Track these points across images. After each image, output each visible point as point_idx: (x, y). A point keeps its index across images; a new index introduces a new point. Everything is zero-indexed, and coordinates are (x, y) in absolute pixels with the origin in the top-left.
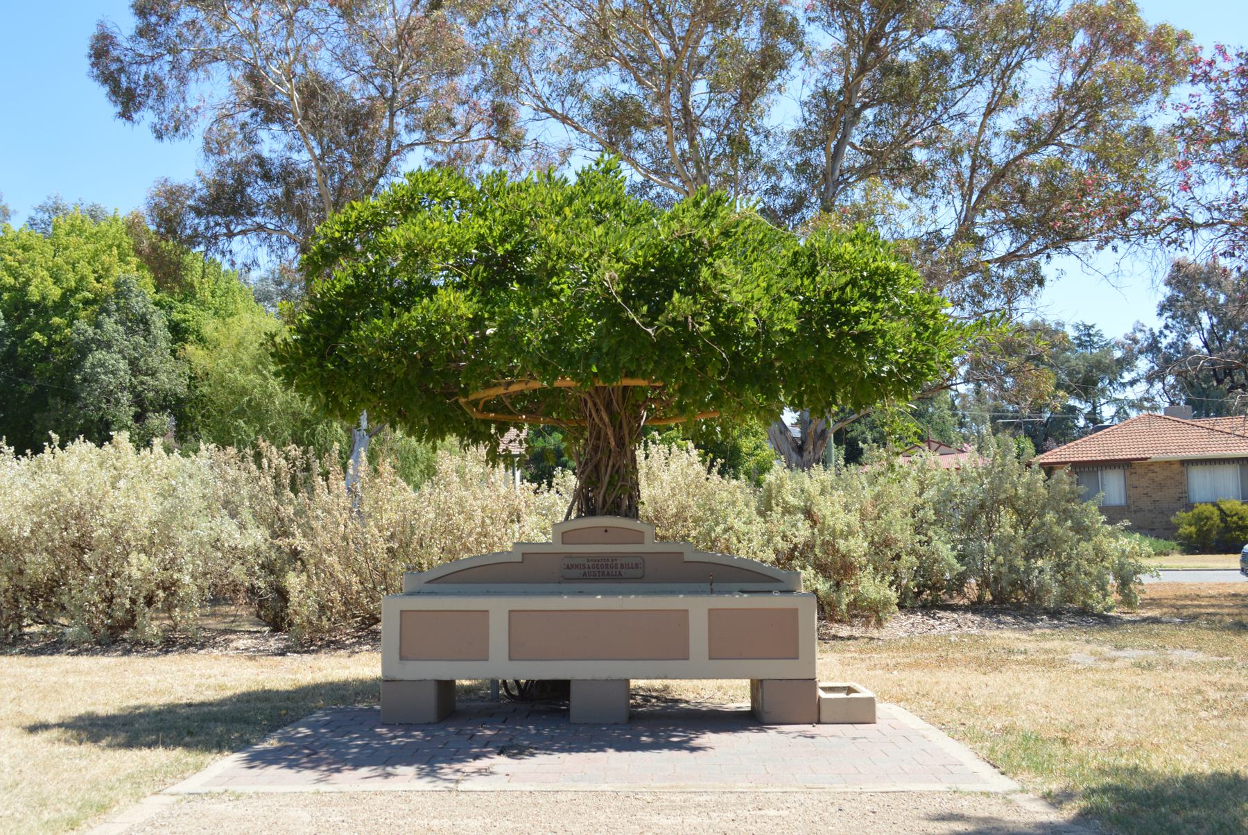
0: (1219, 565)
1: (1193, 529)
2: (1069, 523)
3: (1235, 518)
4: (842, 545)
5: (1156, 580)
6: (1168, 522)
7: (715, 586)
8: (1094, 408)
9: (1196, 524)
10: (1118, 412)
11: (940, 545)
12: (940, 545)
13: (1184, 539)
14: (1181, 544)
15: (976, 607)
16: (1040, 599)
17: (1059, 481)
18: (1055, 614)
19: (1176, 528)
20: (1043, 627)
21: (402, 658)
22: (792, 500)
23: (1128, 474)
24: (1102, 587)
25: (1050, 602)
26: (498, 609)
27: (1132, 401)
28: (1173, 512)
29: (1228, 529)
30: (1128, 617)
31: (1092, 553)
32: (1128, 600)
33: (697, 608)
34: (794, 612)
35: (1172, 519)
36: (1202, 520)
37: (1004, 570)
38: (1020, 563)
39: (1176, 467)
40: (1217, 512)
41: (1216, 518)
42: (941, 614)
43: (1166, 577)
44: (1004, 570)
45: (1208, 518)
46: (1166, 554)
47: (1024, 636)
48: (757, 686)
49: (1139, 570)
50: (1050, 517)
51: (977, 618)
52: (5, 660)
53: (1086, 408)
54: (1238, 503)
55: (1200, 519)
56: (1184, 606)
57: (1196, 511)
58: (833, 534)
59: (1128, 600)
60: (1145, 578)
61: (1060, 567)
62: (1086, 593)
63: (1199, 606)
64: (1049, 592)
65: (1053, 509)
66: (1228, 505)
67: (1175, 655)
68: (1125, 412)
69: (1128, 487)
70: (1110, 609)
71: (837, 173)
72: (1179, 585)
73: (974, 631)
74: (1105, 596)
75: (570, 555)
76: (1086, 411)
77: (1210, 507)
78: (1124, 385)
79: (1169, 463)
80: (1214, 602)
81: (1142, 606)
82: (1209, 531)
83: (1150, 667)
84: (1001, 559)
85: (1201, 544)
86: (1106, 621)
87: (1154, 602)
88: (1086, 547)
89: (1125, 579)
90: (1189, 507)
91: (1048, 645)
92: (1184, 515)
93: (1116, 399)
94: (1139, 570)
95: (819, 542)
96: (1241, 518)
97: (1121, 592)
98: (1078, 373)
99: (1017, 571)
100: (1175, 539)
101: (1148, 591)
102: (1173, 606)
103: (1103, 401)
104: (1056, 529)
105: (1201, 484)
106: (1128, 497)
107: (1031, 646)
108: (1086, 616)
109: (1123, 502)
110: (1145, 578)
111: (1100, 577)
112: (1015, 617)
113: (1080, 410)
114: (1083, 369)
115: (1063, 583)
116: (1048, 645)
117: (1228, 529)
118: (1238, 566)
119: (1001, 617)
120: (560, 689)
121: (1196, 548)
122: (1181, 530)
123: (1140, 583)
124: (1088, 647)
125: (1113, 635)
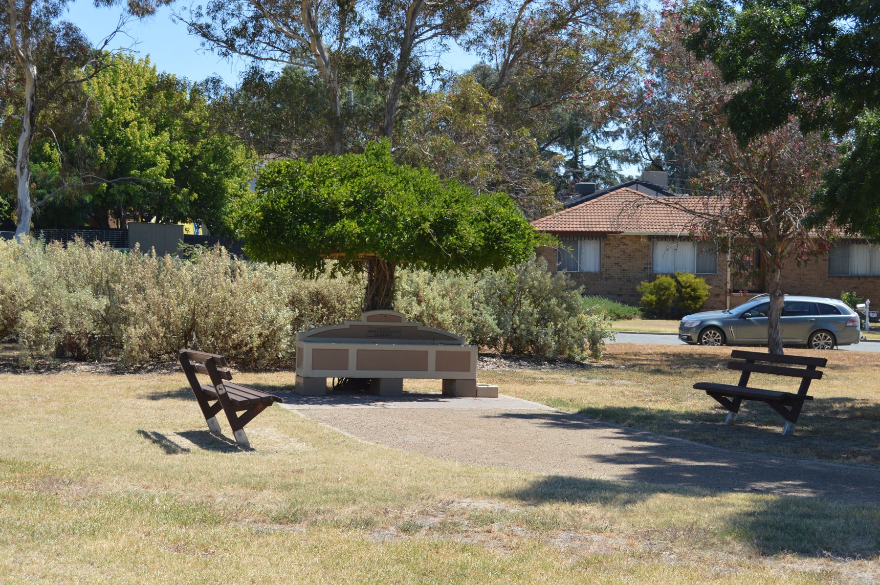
0: (662, 330)
1: (653, 298)
2: (564, 306)
3: (689, 290)
4: (439, 316)
5: (612, 342)
6: (634, 289)
7: (435, 342)
8: (576, 157)
9: (656, 293)
10: (599, 162)
11: (488, 317)
12: (488, 317)
13: (645, 305)
14: (642, 310)
15: (505, 356)
16: (544, 352)
17: (560, 278)
18: (552, 361)
19: (640, 295)
20: (546, 367)
21: (313, 368)
22: (407, 288)
23: (603, 244)
24: (581, 346)
25: (549, 355)
26: (353, 349)
27: (614, 152)
28: (639, 281)
29: (682, 298)
30: (595, 365)
31: (576, 323)
32: (595, 355)
33: (432, 350)
34: (469, 353)
35: (638, 287)
36: (662, 290)
37: (524, 333)
38: (534, 329)
39: (644, 241)
40: (674, 283)
41: (673, 290)
42: (486, 359)
43: (621, 339)
44: (524, 333)
45: (666, 289)
46: (629, 318)
47: (537, 372)
48: (445, 382)
49: (603, 335)
50: (554, 301)
51: (508, 362)
52: (3, 375)
53: (568, 155)
54: (693, 276)
55: (660, 290)
56: (629, 360)
57: (657, 282)
58: (434, 310)
59: (595, 355)
60: (607, 341)
61: (557, 332)
62: (570, 349)
63: (638, 360)
64: (550, 347)
65: (555, 296)
66: (684, 278)
67: (616, 382)
68: (606, 163)
69: (603, 257)
70: (584, 359)
71: (413, 29)
72: (631, 345)
73: (507, 369)
74: (582, 351)
75: (369, 326)
76: (567, 159)
77: (669, 279)
78: (607, 134)
79: (638, 237)
80: (649, 357)
81: (606, 357)
82: (667, 299)
83: (603, 385)
84: (523, 326)
85: (653, 312)
86: (581, 366)
87: (612, 357)
88: (573, 321)
89: (595, 340)
90: (652, 277)
91: (552, 376)
92: (647, 284)
93: (599, 149)
94: (603, 335)
95: (425, 314)
96: (694, 290)
97: (591, 349)
98: (563, 120)
99: (531, 334)
100: (638, 306)
101: (608, 349)
102: (623, 359)
103: (585, 150)
104: (557, 308)
105: (665, 259)
106: (601, 265)
107: (544, 376)
108: (571, 363)
109: (597, 269)
110: (607, 341)
111: (580, 339)
112: (529, 362)
113: (562, 157)
114: (568, 117)
115: (557, 342)
116: (552, 376)
117: (682, 298)
118: (677, 331)
119: (522, 363)
120: (376, 381)
121: (655, 314)
122: (644, 298)
123: (603, 344)
124: (574, 378)
125: (587, 373)
